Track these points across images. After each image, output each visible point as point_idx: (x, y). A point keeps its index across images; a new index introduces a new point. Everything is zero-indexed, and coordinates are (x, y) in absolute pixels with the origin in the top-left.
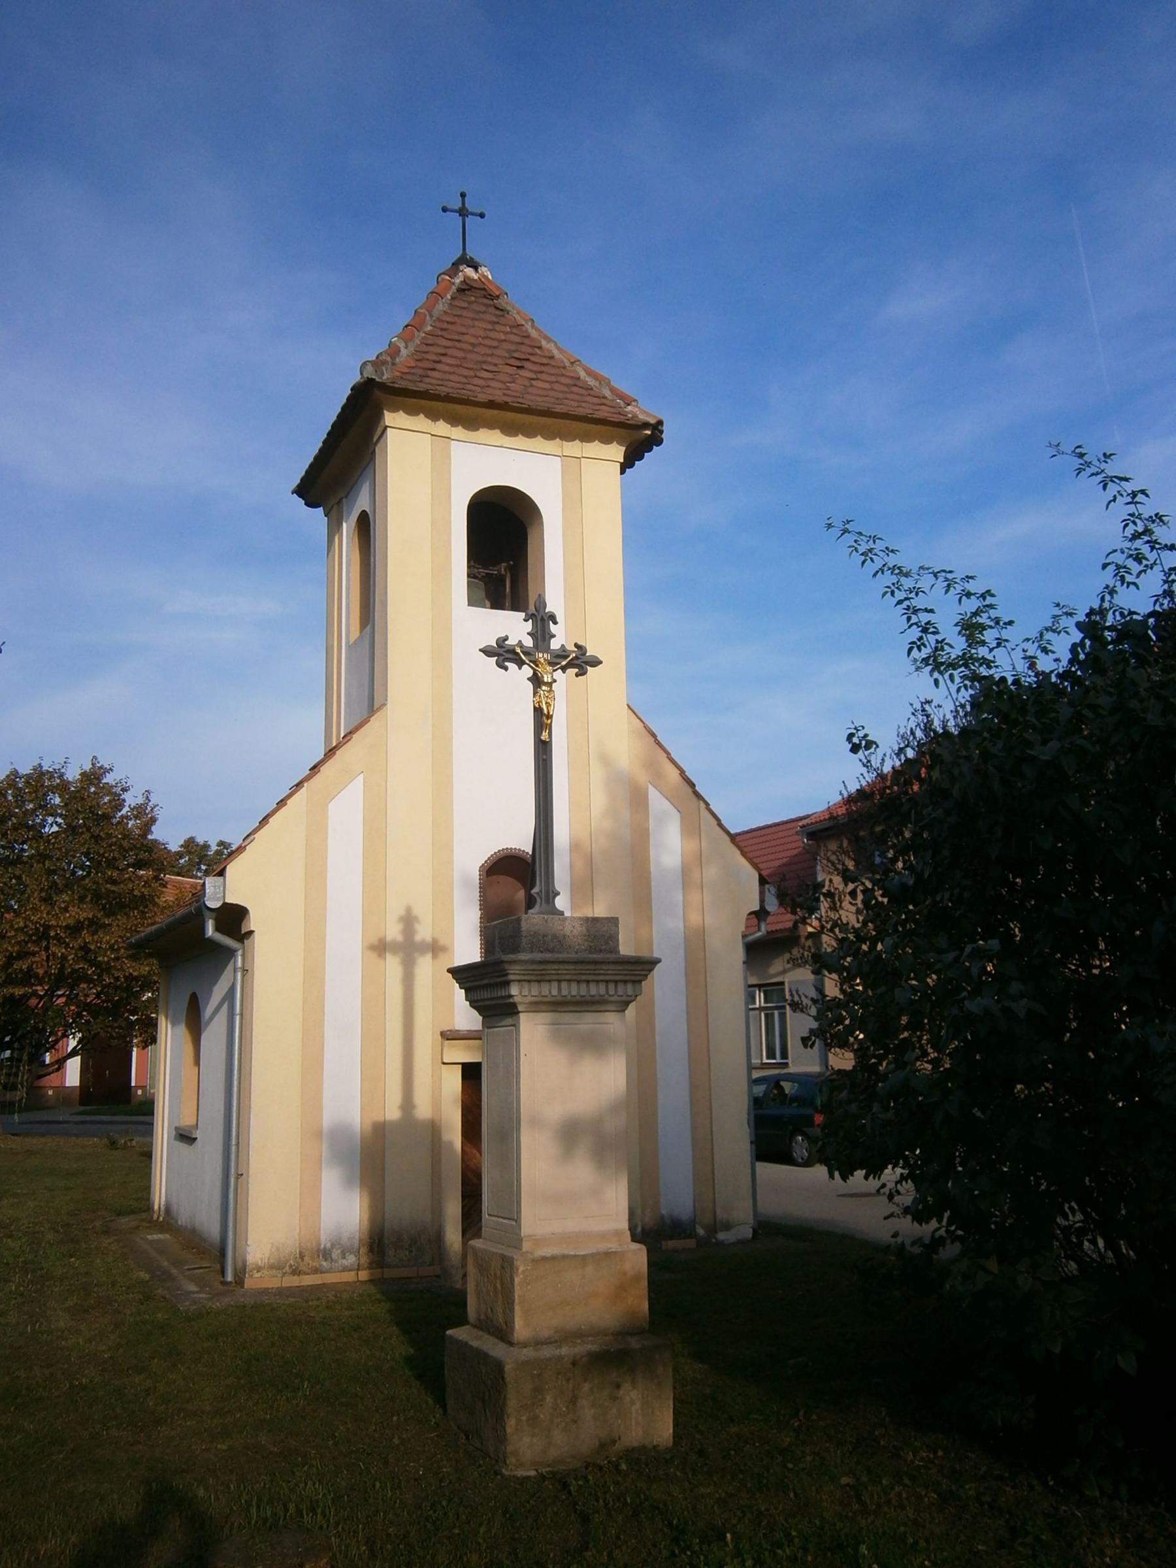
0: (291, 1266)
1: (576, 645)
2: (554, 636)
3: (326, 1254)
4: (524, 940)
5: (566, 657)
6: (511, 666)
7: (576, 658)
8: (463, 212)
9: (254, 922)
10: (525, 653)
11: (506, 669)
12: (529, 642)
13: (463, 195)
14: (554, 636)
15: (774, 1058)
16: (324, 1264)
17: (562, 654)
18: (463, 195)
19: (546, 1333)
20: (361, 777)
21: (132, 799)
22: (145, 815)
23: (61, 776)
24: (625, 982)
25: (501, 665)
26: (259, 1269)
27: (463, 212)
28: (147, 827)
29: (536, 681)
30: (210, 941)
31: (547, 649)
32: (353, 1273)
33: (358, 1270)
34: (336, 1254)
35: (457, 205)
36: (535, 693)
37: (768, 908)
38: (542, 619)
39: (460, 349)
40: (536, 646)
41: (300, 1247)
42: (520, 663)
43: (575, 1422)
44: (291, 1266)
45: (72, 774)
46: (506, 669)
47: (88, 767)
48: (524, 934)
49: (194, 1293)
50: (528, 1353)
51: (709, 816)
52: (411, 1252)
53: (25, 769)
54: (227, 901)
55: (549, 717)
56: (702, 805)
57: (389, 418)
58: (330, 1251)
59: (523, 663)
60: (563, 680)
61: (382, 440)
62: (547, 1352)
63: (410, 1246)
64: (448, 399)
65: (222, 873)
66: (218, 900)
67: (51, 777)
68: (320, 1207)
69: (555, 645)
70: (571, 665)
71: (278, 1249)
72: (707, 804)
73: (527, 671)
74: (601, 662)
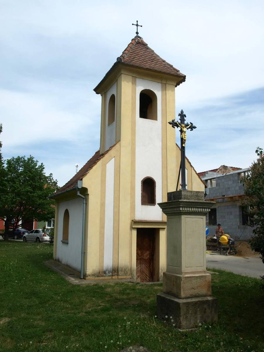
0: (97, 275)
1: (191, 123)
2: (185, 120)
3: (105, 272)
4: (183, 196)
5: (188, 126)
6: (176, 127)
7: (191, 126)
8: (137, 25)
9: (89, 192)
10: (179, 124)
11: (174, 128)
12: (179, 121)
13: (137, 21)
14: (185, 120)
15: (50, 226)
16: (104, 275)
17: (187, 125)
18: (137, 21)
19: (188, 296)
20: (114, 159)
21: (39, 164)
22: (42, 167)
23: (24, 159)
24: (185, 207)
25: (173, 127)
26: (89, 275)
27: (137, 25)
28: (42, 170)
29: (181, 131)
30: (79, 195)
31: (184, 123)
32: (111, 277)
33: (112, 276)
34: (107, 272)
35: (136, 24)
36: (181, 134)
37: (207, 193)
38: (183, 116)
39: (138, 56)
40: (181, 122)
41: (99, 271)
42: (178, 126)
43: (196, 318)
44: (97, 275)
45: (26, 159)
46: (174, 128)
47: (29, 157)
48: (183, 195)
49: (73, 280)
50: (185, 301)
51: (194, 171)
52: (124, 272)
53: (16, 157)
54: (83, 186)
55: (185, 140)
56: (192, 168)
57: (122, 72)
58: (106, 272)
59: (179, 126)
60: (188, 132)
61: (121, 76)
62: (189, 300)
63: (124, 271)
64: (137, 67)
65: (82, 180)
66: (81, 186)
67: (13, 160)
68: (104, 260)
69: (186, 122)
70: (189, 128)
71: (94, 271)
72: (193, 168)
73: (179, 128)
74: (196, 128)
